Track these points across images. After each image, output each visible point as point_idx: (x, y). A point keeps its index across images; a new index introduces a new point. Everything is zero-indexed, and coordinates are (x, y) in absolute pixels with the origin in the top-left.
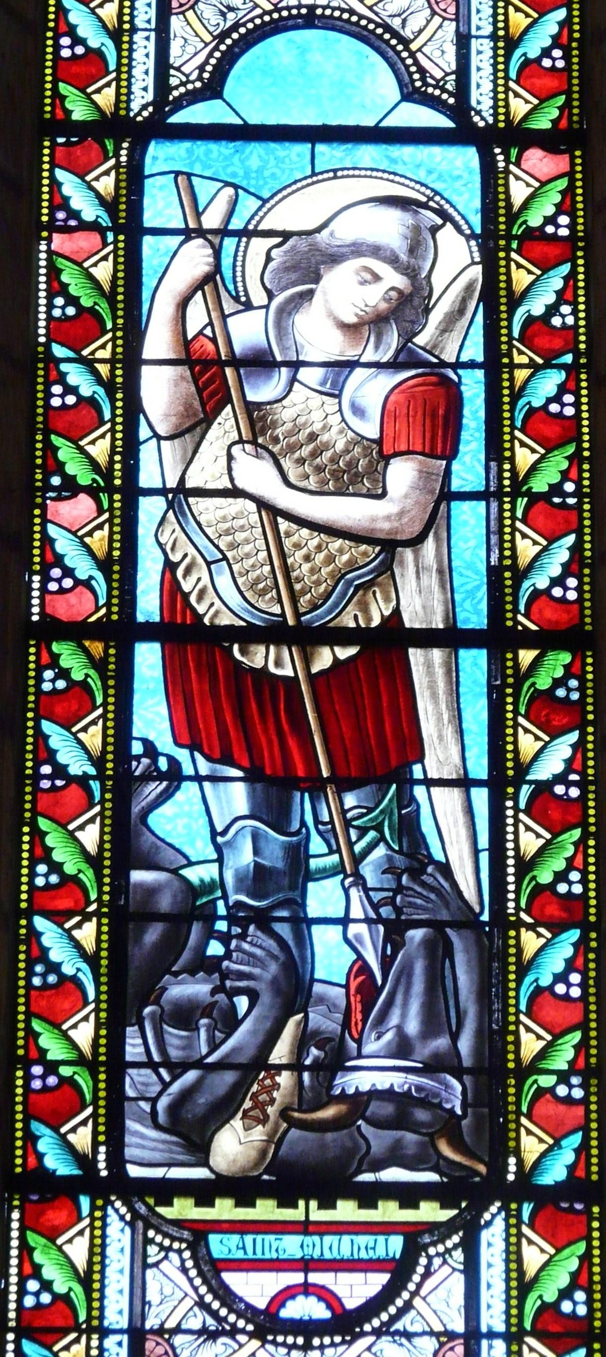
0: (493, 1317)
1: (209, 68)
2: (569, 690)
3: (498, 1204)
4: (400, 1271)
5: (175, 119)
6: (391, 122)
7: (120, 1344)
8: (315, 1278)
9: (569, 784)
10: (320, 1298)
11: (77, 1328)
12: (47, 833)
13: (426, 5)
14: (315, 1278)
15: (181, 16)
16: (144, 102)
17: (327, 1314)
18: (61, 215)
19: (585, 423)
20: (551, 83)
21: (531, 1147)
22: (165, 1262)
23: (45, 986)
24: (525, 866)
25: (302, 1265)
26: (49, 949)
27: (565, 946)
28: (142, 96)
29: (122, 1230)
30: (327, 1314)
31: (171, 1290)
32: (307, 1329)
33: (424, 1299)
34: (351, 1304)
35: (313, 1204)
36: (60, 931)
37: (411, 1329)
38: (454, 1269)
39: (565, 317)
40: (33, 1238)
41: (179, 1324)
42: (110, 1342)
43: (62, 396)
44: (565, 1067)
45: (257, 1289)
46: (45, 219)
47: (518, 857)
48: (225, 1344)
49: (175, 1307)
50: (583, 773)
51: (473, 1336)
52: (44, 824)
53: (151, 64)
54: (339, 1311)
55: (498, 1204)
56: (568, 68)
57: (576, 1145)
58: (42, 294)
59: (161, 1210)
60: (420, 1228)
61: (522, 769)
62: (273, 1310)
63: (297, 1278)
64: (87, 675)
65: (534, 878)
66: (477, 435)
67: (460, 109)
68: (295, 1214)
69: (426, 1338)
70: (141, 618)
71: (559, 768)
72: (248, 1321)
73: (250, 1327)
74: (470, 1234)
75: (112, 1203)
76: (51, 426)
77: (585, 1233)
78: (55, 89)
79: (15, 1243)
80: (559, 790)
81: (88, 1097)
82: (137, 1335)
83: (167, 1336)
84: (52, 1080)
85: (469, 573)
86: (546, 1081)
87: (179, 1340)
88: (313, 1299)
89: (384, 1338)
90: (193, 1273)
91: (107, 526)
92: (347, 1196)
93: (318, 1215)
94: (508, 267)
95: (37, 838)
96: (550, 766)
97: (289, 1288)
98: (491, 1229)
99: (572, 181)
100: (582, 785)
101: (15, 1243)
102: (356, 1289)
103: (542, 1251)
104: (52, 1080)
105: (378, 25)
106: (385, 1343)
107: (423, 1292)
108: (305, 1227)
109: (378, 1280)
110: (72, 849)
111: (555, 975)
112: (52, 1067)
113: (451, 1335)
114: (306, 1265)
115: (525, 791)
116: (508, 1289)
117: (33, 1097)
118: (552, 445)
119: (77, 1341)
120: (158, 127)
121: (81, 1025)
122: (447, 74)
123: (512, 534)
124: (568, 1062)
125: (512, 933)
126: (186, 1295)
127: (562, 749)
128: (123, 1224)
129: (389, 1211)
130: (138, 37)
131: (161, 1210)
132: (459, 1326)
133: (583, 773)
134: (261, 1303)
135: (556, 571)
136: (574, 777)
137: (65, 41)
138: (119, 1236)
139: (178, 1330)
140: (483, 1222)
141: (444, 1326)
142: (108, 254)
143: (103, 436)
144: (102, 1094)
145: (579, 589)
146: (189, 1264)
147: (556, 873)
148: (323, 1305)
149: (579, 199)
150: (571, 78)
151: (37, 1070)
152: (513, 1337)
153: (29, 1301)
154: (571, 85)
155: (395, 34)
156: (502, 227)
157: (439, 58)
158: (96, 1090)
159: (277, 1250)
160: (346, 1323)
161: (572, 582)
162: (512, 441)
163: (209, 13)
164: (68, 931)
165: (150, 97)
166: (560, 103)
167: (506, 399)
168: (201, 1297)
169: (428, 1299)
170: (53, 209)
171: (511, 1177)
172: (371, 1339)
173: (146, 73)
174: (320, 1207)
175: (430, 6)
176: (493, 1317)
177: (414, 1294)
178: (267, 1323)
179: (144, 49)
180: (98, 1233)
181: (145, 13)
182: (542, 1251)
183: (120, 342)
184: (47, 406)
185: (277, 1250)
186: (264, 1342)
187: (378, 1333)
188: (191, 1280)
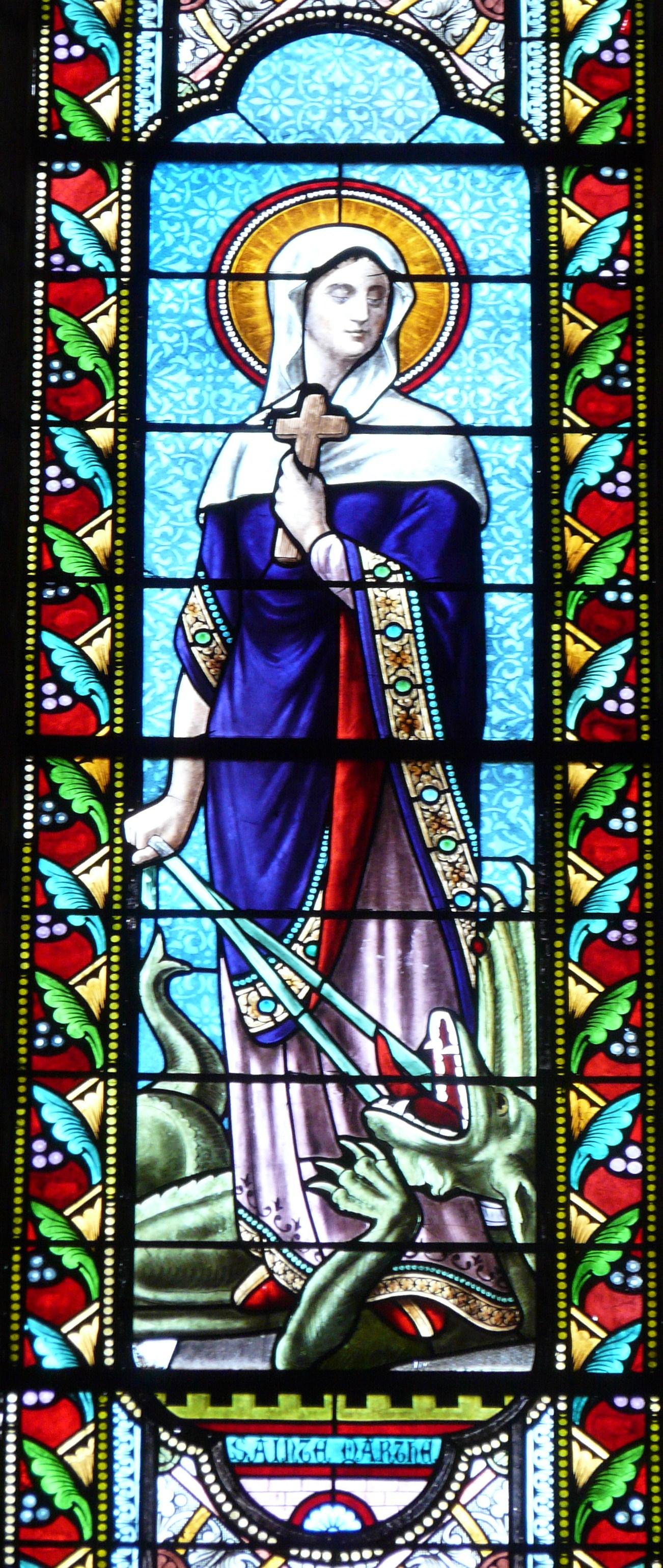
0: (540, 1528)
1: (223, 74)
2: (626, 1045)
3: (546, 1400)
4: (438, 1478)
5: (186, 137)
6: (428, 137)
7: (129, 1558)
8: (343, 1485)
9: (621, 590)
10: (348, 1507)
11: (93, 1072)
12: (45, 991)
13: (470, 5)
14: (343, 1485)
15: (191, 16)
16: (150, 113)
17: (356, 1526)
18: (57, 259)
19: (642, 407)
20: (609, 303)
21: (582, 1344)
22: (178, 1469)
23: (54, 824)
24: (578, 1024)
25: (328, 1471)
26: (61, 668)
27: (612, 446)
28: (148, 106)
29: (131, 1431)
30: (356, 1526)
31: (183, 1497)
32: (337, 1542)
33: (464, 1506)
34: (382, 1514)
35: (341, 1399)
36: (60, 1218)
37: (449, 1541)
38: (498, 1475)
39: (627, 822)
40: (30, 1447)
41: (195, 1539)
42: (118, 1556)
43: (50, 925)
44: (616, 910)
45: (278, 1497)
46: (39, 264)
47: (565, 668)
48: (245, 1562)
49: (190, 1519)
50: (634, 578)
51: (518, 1547)
52: (43, 981)
53: (158, 69)
54: (369, 1523)
55: (546, 1400)
56: (640, 946)
57: (636, 1458)
58: (35, 463)
59: (173, 1409)
60: (459, 1428)
61: (570, 579)
62: (296, 1522)
63: (324, 1485)
64: (91, 808)
65: (587, 1037)
66: (525, 659)
67: (508, 122)
68: (323, 1414)
69: (467, 1552)
70: (147, 732)
71: (611, 572)
72: (270, 1534)
73: (273, 1541)
74: (517, 1426)
75: (117, 1399)
76: (54, 196)
77: (635, 857)
78: (48, 214)
79: (11, 1458)
80: (611, 596)
81: (95, 1294)
82: (146, 1542)
83: (181, 1552)
84: (60, 929)
85: (513, 482)
86: (598, 926)
87: (194, 1557)
88: (339, 1510)
89: (419, 1553)
90: (210, 1479)
91: (91, 1442)
92: (377, 1390)
93: (348, 1414)
94: (563, 643)
95: (44, 547)
96: (601, 571)
97: (317, 1495)
98: (538, 1429)
99: (644, 1214)
100: (636, 588)
101: (11, 1458)
102: (388, 1498)
103: (595, 1455)
104: (60, 929)
105: (415, 30)
106: (419, 1557)
107: (464, 1499)
108: (333, 1428)
109: (414, 1488)
110: (86, 451)
111: (611, 1148)
112: (60, 916)
113: (496, 1548)
114: (334, 1471)
115: (575, 597)
116: (557, 1499)
117: (44, 717)
118: (620, 1443)
119: (93, 1089)
120: (163, 148)
121: (87, 1096)
122: (493, 84)
123: (561, 92)
124: (624, 1362)
125: (554, 440)
126: (202, 1505)
127: (612, 446)
128: (131, 1424)
129: (423, 1407)
130: (143, 38)
131: (173, 1409)
132: (501, 1536)
133: (634, 578)
134: (284, 1514)
135: (611, 680)
136: (624, 582)
137: (61, 39)
138: (128, 1439)
139: (193, 1545)
140: (529, 1421)
141: (487, 1537)
142: (104, 630)
143: (89, 1321)
144: (109, 1291)
145: (632, 484)
146: (206, 1468)
147: (609, 1032)
148: (351, 1515)
149: (644, 616)
150: (638, 509)
151: (44, 919)
152: (559, 1549)
153: (26, 1516)
154: (645, 1193)
155: (434, 40)
156: (554, 266)
157: (481, 70)
158: (102, 1287)
159: (301, 1454)
160: (378, 1535)
161: (627, 693)
162: (559, 316)
163: (220, 11)
164: (68, 1219)
165: (157, 107)
166: (633, 1338)
167: (561, 1150)
168: (218, 1506)
169: (469, 1508)
170: (49, 252)
171: (561, 1366)
172: (406, 1553)
173: (152, 80)
174: (350, 1404)
175: (474, 6)
176: (540, 1528)
177: (452, 1504)
178: (290, 1535)
179: (150, 49)
180: (103, 1446)
181: (150, 12)
182: (595, 1455)
183: (119, 626)
184: (38, 708)
185: (301, 1454)
186: (288, 1557)
187: (413, 1546)
188: (207, 1488)
